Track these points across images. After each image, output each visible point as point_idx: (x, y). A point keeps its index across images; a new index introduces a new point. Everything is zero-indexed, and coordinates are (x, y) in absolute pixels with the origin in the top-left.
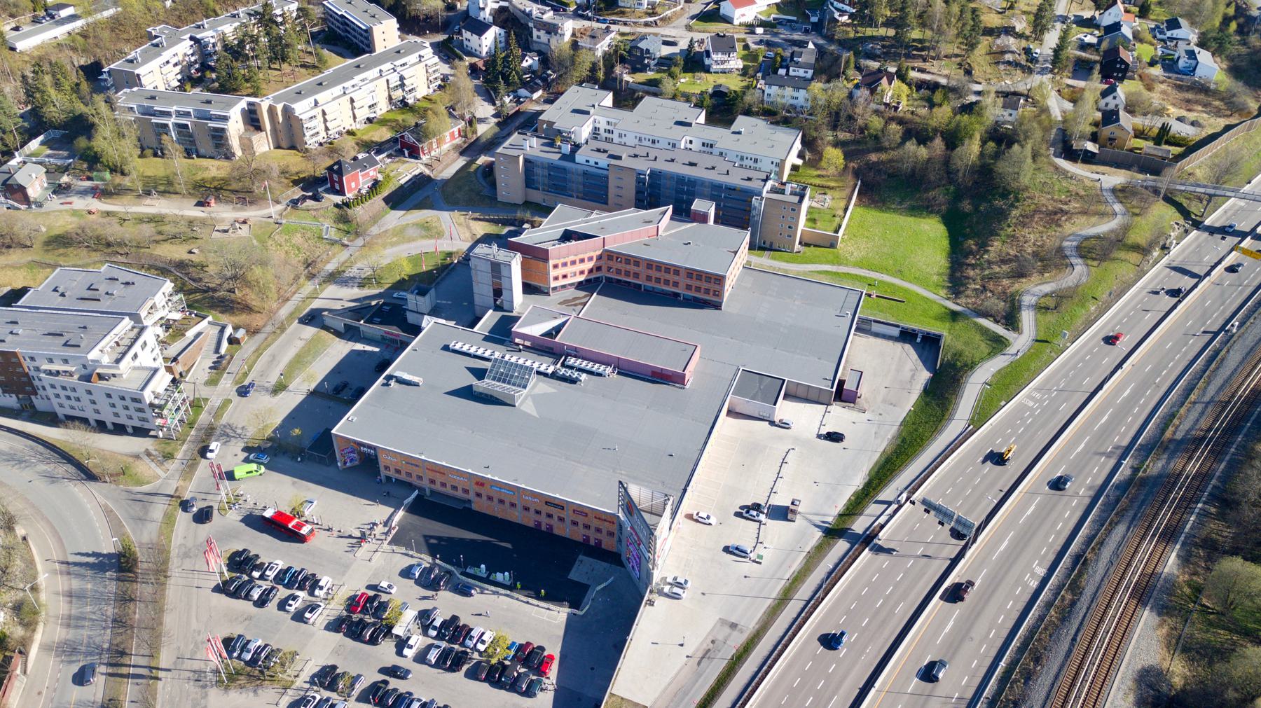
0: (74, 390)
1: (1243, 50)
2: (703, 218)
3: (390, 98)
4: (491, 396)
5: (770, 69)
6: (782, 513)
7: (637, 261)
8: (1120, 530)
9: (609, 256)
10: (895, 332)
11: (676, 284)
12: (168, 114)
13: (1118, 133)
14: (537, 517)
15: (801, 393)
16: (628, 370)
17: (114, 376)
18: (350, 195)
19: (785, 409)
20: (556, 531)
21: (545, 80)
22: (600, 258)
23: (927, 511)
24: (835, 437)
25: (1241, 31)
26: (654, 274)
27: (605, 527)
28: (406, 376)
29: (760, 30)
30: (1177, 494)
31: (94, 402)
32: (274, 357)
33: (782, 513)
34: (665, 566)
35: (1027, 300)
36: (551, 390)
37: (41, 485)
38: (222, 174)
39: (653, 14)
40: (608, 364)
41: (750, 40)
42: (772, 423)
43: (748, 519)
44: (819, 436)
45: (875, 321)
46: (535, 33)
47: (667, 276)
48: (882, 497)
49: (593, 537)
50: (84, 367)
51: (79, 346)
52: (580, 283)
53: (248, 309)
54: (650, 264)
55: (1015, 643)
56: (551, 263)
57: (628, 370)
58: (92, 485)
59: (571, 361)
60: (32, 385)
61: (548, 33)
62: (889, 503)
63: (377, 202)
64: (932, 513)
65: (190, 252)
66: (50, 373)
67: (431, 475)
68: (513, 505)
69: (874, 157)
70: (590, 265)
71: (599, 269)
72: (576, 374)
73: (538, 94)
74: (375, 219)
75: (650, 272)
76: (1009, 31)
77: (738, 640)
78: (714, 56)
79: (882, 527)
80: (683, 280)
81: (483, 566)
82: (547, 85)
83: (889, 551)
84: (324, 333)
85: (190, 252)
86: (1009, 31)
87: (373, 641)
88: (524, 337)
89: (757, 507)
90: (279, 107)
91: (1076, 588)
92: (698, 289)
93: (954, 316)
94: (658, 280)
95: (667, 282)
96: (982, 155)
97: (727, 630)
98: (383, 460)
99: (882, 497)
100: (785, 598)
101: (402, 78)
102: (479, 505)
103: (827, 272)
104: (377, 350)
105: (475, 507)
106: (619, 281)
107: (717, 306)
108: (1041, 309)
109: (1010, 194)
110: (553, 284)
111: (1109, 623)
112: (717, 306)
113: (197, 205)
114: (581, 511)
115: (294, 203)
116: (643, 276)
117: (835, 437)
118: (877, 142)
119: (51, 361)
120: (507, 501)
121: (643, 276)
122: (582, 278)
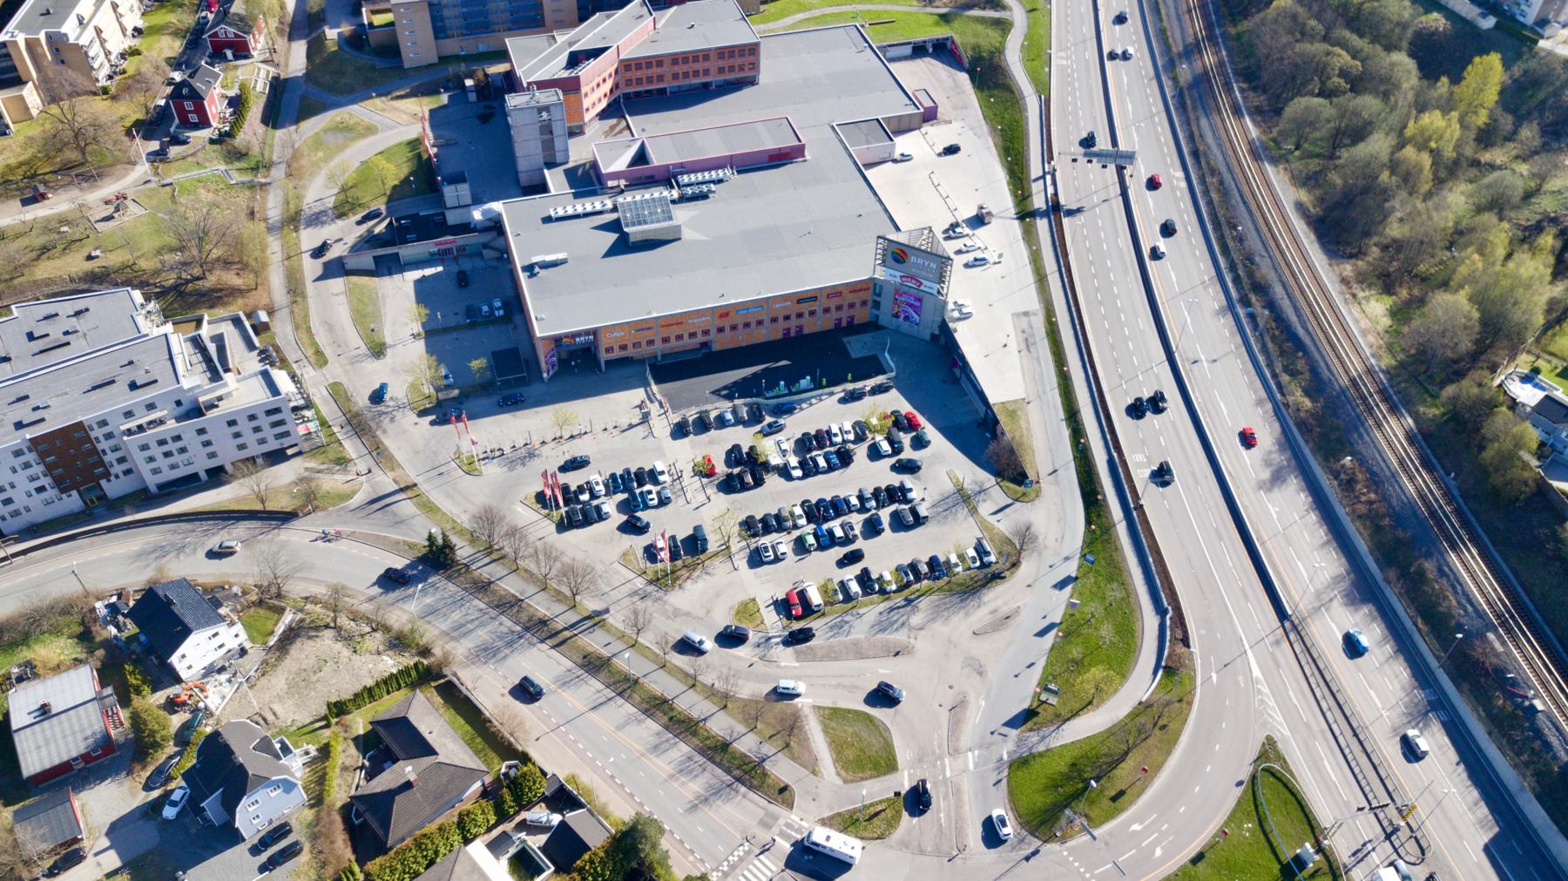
0: (178, 438)
4: (646, 241)
6: (979, 220)
7: (658, 61)
8: (1204, 122)
9: (626, 66)
10: (908, 50)
16: (748, 164)
17: (220, 399)
19: (903, 144)
20: (806, 331)
23: (1090, 161)
24: (952, 150)
28: (550, 258)
30: (1217, 83)
32: (330, 327)
33: (979, 220)
36: (694, 213)
40: (722, 167)
42: (895, 161)
43: (957, 238)
44: (939, 155)
45: (890, 46)
48: (1033, 176)
49: (844, 315)
50: (179, 403)
51: (156, 381)
52: (603, 111)
53: (235, 292)
54: (676, 59)
55: (1209, 227)
56: (584, 90)
57: (748, 164)
58: (296, 524)
59: (685, 179)
60: (102, 463)
62: (1043, 177)
64: (1095, 160)
65: (90, 258)
66: (129, 432)
68: (760, 323)
70: (610, 84)
71: (616, 86)
72: (705, 188)
75: (676, 69)
77: (1039, 322)
79: (1056, 194)
80: (713, 65)
81: (782, 383)
83: (1079, 210)
84: (354, 279)
85: (90, 258)
87: (759, 482)
88: (616, 175)
89: (954, 226)
90: (42, 37)
91: (1214, 172)
94: (686, 75)
95: (696, 73)
97: (1025, 319)
99: (1033, 176)
102: (720, 343)
103: (801, 22)
104: (440, 269)
105: (716, 347)
106: (638, 94)
113: (25, 202)
114: (834, 292)
115: (159, 157)
116: (668, 77)
117: (952, 150)
119: (129, 414)
120: (753, 322)
122: (604, 104)
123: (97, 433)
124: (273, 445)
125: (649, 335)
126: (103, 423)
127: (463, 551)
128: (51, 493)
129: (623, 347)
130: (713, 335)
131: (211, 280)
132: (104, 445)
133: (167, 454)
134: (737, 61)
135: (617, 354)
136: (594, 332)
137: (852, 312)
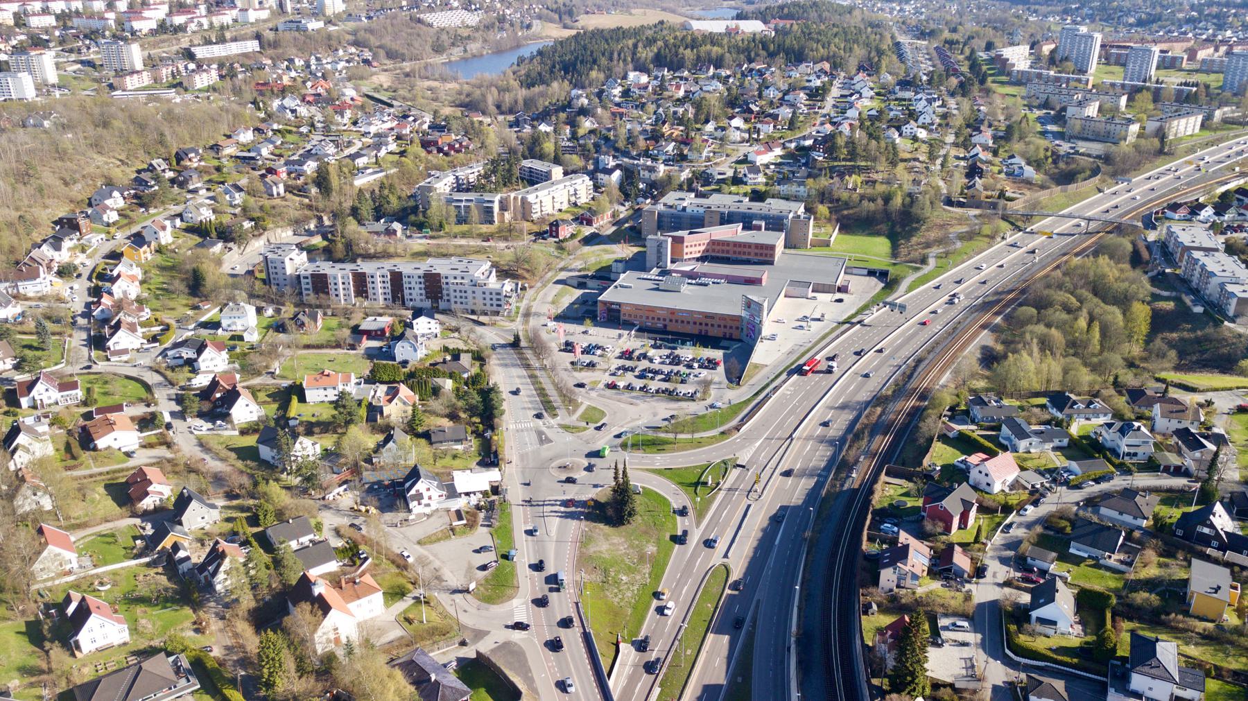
1: (1056, 171)
2: (758, 228)
3: (569, 201)
5: (784, 180)
10: (865, 272)
11: (749, 254)
12: (461, 201)
13: (976, 193)
14: (700, 327)
15: (820, 288)
18: (561, 238)
20: (710, 334)
21: (651, 194)
22: (708, 244)
25: (1055, 162)
26: (738, 249)
27: (734, 324)
29: (772, 167)
31: (474, 298)
34: (766, 331)
35: (931, 255)
37: (173, 613)
38: (489, 231)
39: (710, 161)
41: (767, 171)
46: (642, 173)
47: (745, 250)
49: (728, 331)
56: (685, 244)
61: (650, 171)
63: (576, 241)
67: (647, 314)
68: (688, 322)
69: (845, 212)
70: (702, 248)
71: (708, 251)
73: (648, 201)
74: (575, 249)
76: (916, 160)
77: (802, 350)
78: (749, 176)
80: (753, 251)
82: (653, 197)
86: (916, 160)
90: (520, 197)
92: (761, 255)
93: (894, 264)
94: (740, 253)
95: (744, 253)
96: (903, 204)
98: (624, 309)
100: (823, 338)
101: (575, 190)
107: (771, 263)
108: (937, 257)
109: (919, 220)
110: (685, 257)
111: (971, 332)
112: (771, 263)
116: (731, 252)
118: (847, 205)
119: (455, 278)
121: (731, 252)
123: (444, 281)
124: (495, 308)
125: (640, 313)
126: (446, 278)
127: (523, 344)
128: (424, 297)
129: (630, 315)
130: (667, 322)
131: (520, 272)
132: (444, 286)
133: (461, 297)
134: (765, 252)
135: (626, 318)
136: (619, 304)
137: (731, 331)
